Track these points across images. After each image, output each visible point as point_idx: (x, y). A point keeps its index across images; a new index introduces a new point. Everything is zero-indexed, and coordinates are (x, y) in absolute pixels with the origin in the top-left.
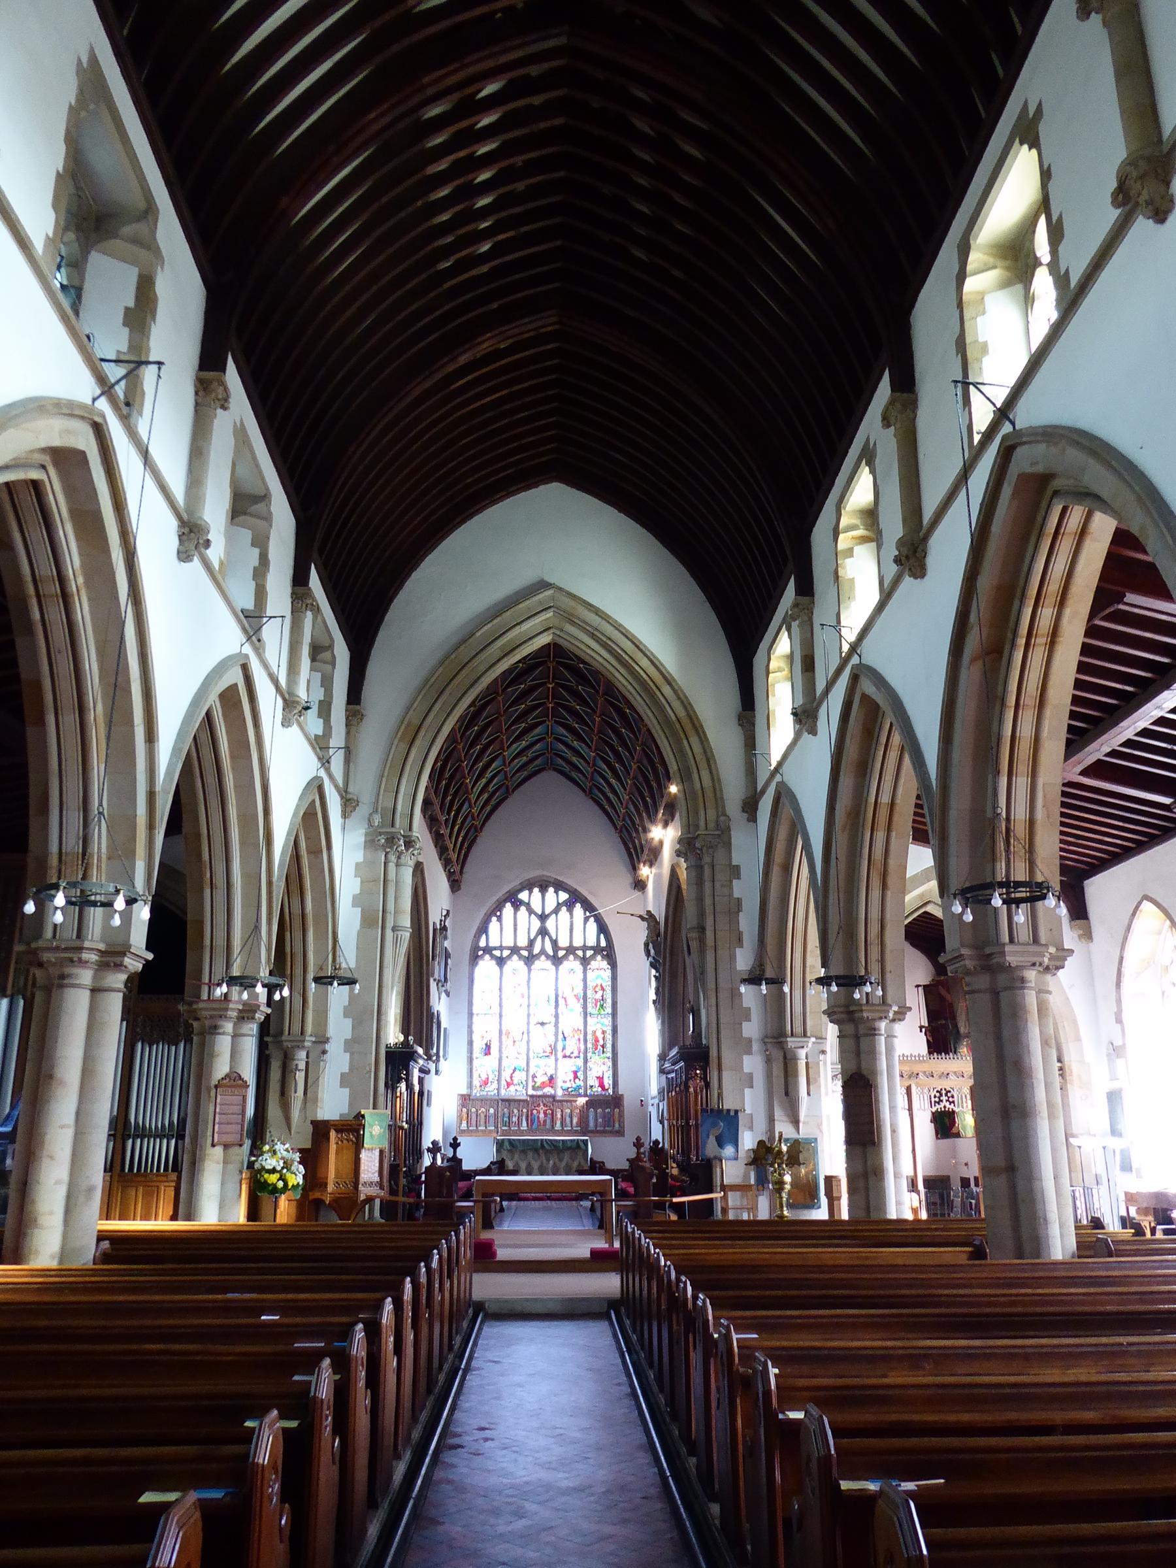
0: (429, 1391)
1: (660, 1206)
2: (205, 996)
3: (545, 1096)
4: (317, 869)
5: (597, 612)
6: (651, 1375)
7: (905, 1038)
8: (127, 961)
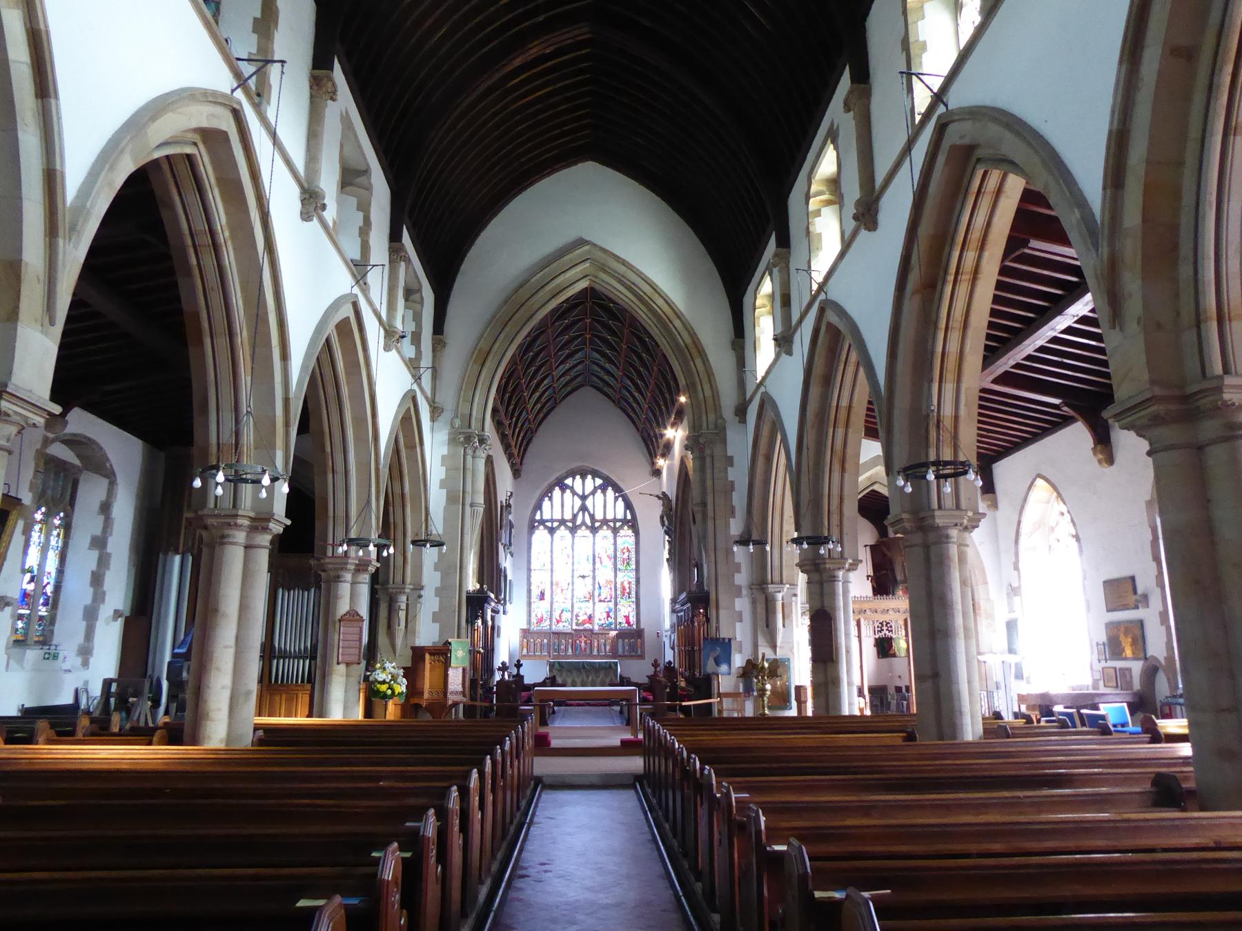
0: (504, 837)
1: (672, 709)
2: (330, 553)
3: (585, 630)
4: (413, 460)
5: (624, 263)
6: (667, 826)
7: (856, 584)
8: (271, 525)
